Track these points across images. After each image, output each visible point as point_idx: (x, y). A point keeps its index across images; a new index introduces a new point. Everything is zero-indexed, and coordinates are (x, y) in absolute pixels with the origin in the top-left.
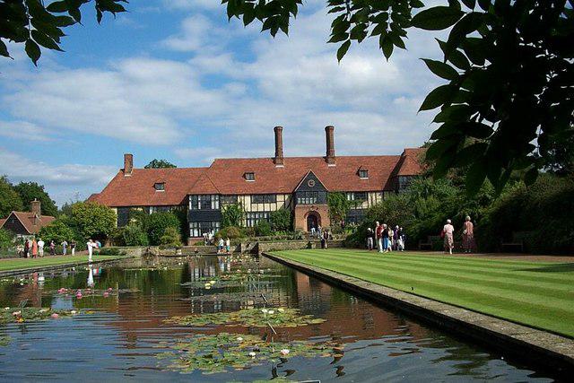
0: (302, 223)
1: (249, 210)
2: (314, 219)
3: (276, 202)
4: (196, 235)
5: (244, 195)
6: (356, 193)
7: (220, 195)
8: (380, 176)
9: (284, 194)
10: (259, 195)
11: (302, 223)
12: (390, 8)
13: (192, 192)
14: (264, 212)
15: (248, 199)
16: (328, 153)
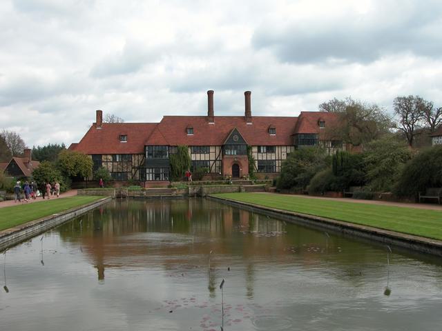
1: (256, 159)
5: (107, 155)
6: (267, 146)
10: (197, 146)
13: (149, 143)
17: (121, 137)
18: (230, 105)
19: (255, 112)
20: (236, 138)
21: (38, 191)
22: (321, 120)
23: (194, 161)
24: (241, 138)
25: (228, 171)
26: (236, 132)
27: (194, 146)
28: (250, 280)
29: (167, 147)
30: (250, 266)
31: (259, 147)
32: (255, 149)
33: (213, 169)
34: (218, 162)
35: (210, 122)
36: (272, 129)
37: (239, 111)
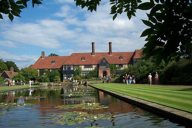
0: (101, 75)
1: (83, 70)
2: (105, 73)
3: (92, 68)
4: (66, 78)
5: (82, 65)
6: (119, 64)
7: (74, 65)
8: (127, 59)
9: (95, 65)
10: (87, 65)
11: (101, 75)
13: (64, 64)
14: (88, 71)
15: (83, 67)
16: (110, 51)
21: (131, 3)
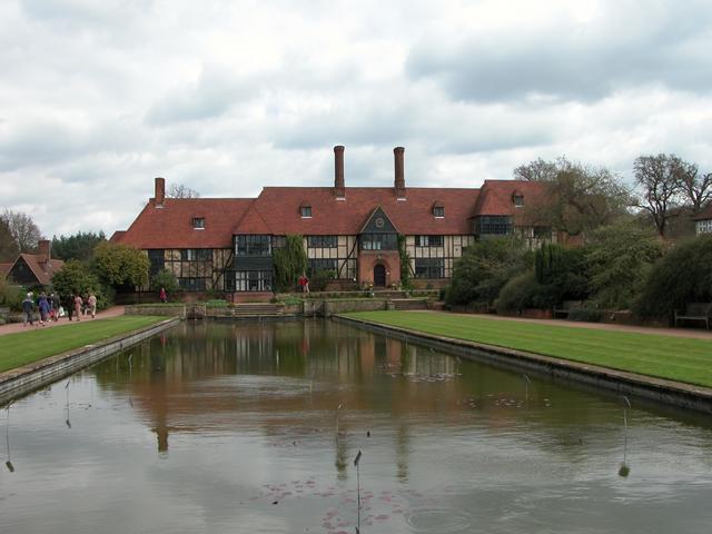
1: (413, 256)
5: (172, 249)
6: (430, 236)
10: (318, 236)
12: (62, 309)
13: (240, 230)
17: (195, 221)
18: (370, 170)
19: (410, 181)
20: (380, 223)
22: (518, 194)
23: (312, 260)
24: (388, 222)
25: (368, 276)
26: (380, 213)
27: (312, 236)
28: (403, 452)
29: (269, 238)
30: (403, 429)
31: (417, 238)
32: (410, 241)
33: (344, 272)
34: (351, 262)
35: (338, 196)
36: (439, 208)
37: (386, 178)
